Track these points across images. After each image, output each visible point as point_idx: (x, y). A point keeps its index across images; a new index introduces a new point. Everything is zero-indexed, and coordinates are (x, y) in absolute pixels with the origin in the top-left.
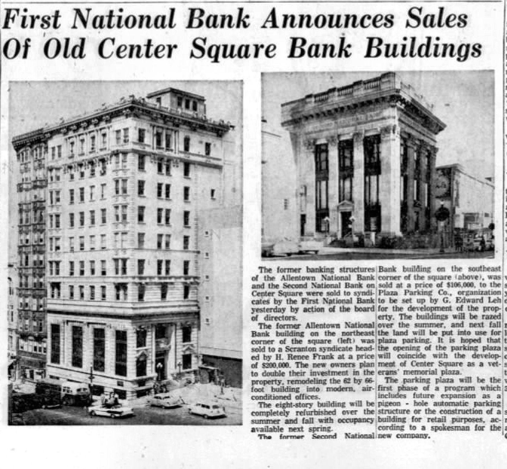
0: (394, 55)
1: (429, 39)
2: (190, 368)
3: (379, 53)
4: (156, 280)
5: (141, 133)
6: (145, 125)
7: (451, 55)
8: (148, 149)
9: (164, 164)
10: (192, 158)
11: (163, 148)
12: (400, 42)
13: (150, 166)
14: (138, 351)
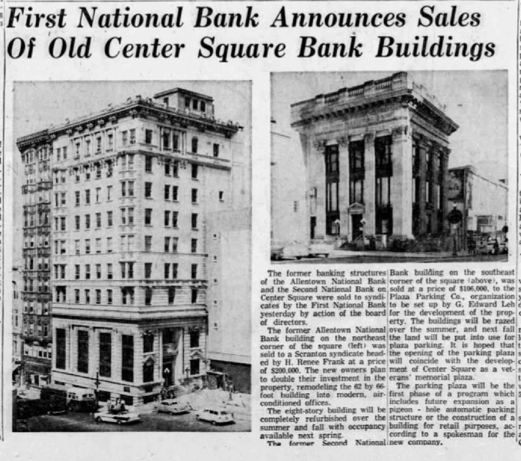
0: (406, 54)
1: (442, 38)
2: (198, 373)
3: (390, 52)
4: (164, 284)
5: (148, 133)
6: (152, 126)
7: (464, 54)
8: (155, 151)
9: (171, 166)
10: (200, 160)
11: (170, 150)
12: (412, 42)
13: (158, 168)
14: (145, 356)
